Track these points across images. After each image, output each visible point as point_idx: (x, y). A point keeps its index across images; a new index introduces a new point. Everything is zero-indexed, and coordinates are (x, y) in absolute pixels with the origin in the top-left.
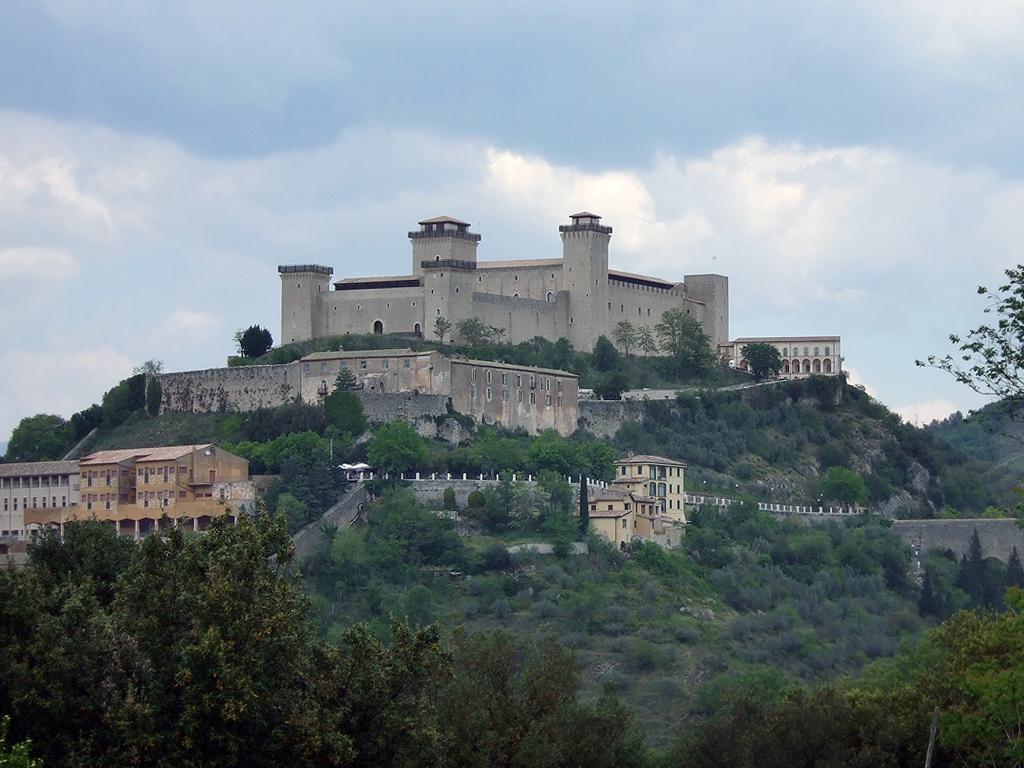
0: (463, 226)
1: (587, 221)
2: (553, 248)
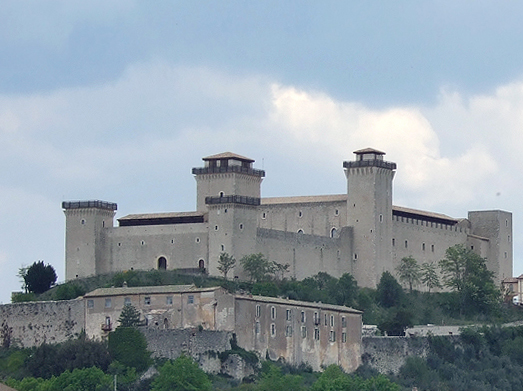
0: (247, 162)
1: (371, 157)
2: (337, 184)
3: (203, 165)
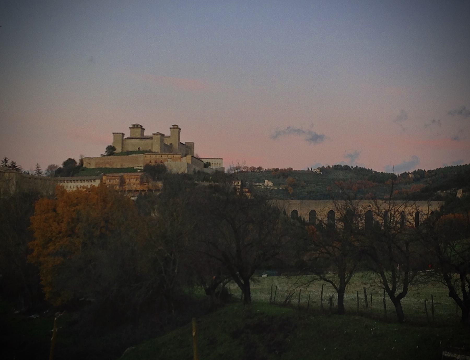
0: (142, 126)
3: (131, 126)
